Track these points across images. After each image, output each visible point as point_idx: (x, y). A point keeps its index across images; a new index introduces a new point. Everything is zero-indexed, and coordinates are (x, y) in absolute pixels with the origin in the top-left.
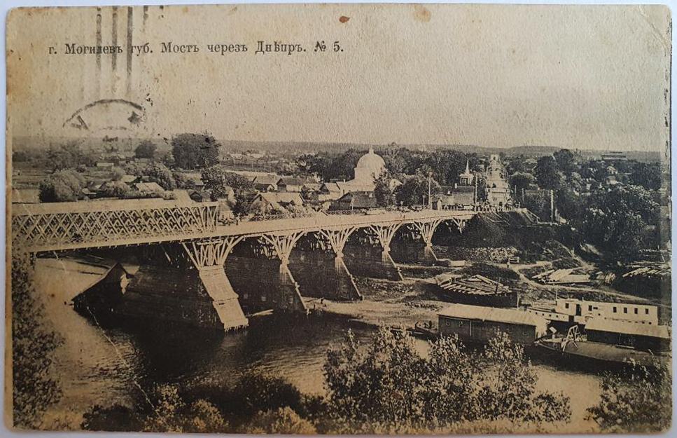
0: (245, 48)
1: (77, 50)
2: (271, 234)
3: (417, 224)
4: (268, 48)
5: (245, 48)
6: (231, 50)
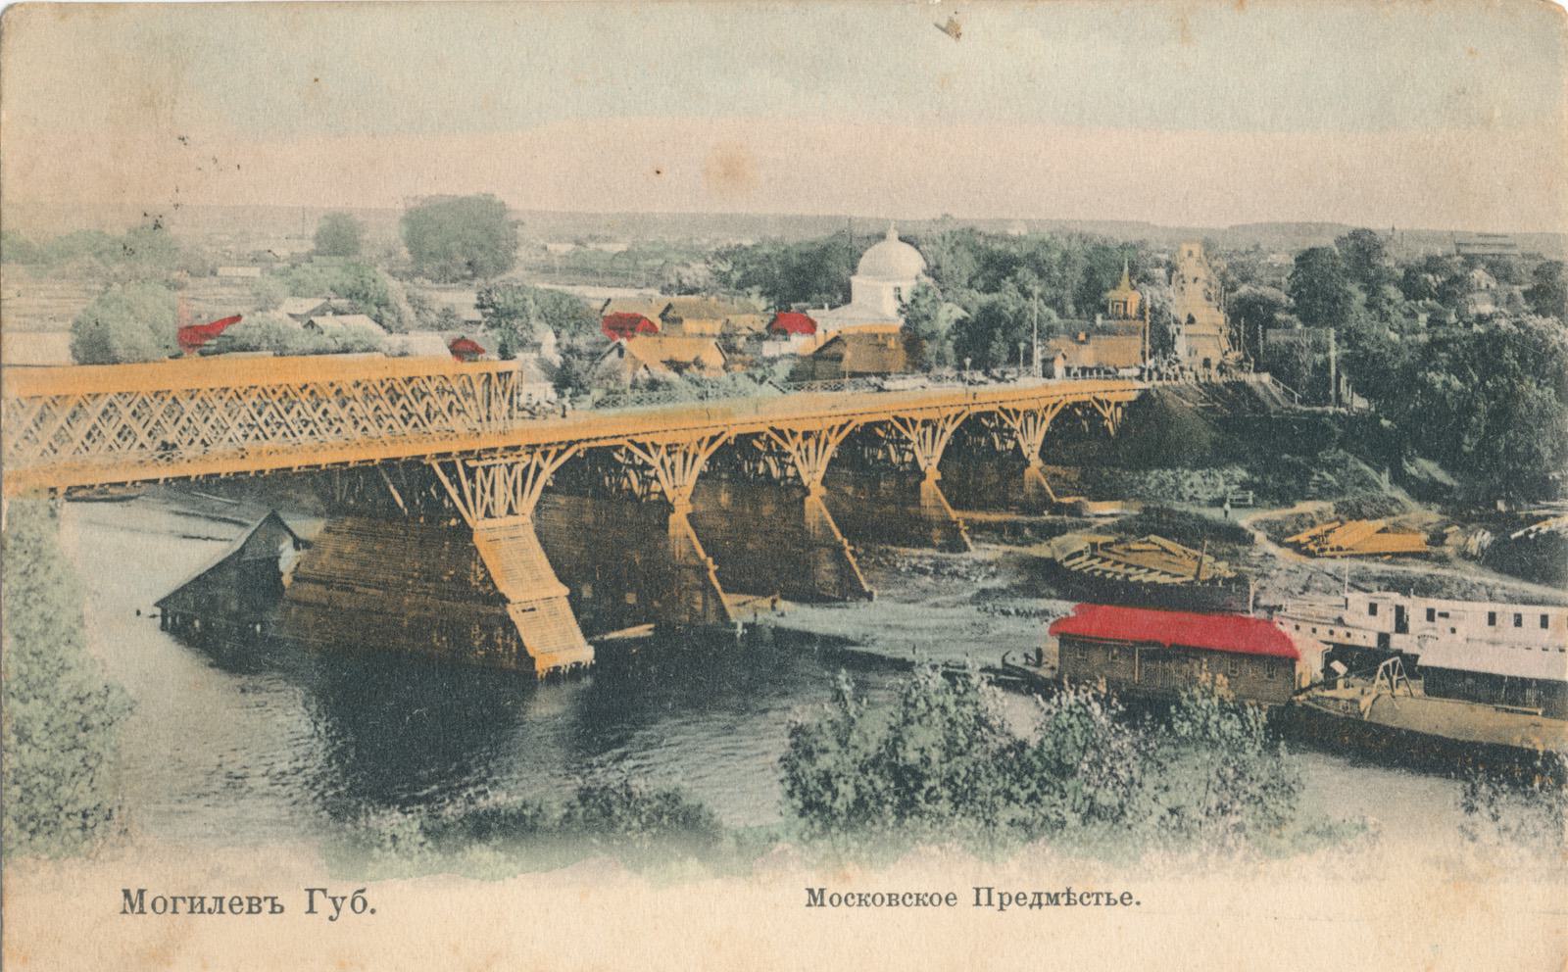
0: (277, 908)
1: (883, 899)
2: (647, 440)
3: (1007, 412)
5: (277, 908)
6: (237, 909)
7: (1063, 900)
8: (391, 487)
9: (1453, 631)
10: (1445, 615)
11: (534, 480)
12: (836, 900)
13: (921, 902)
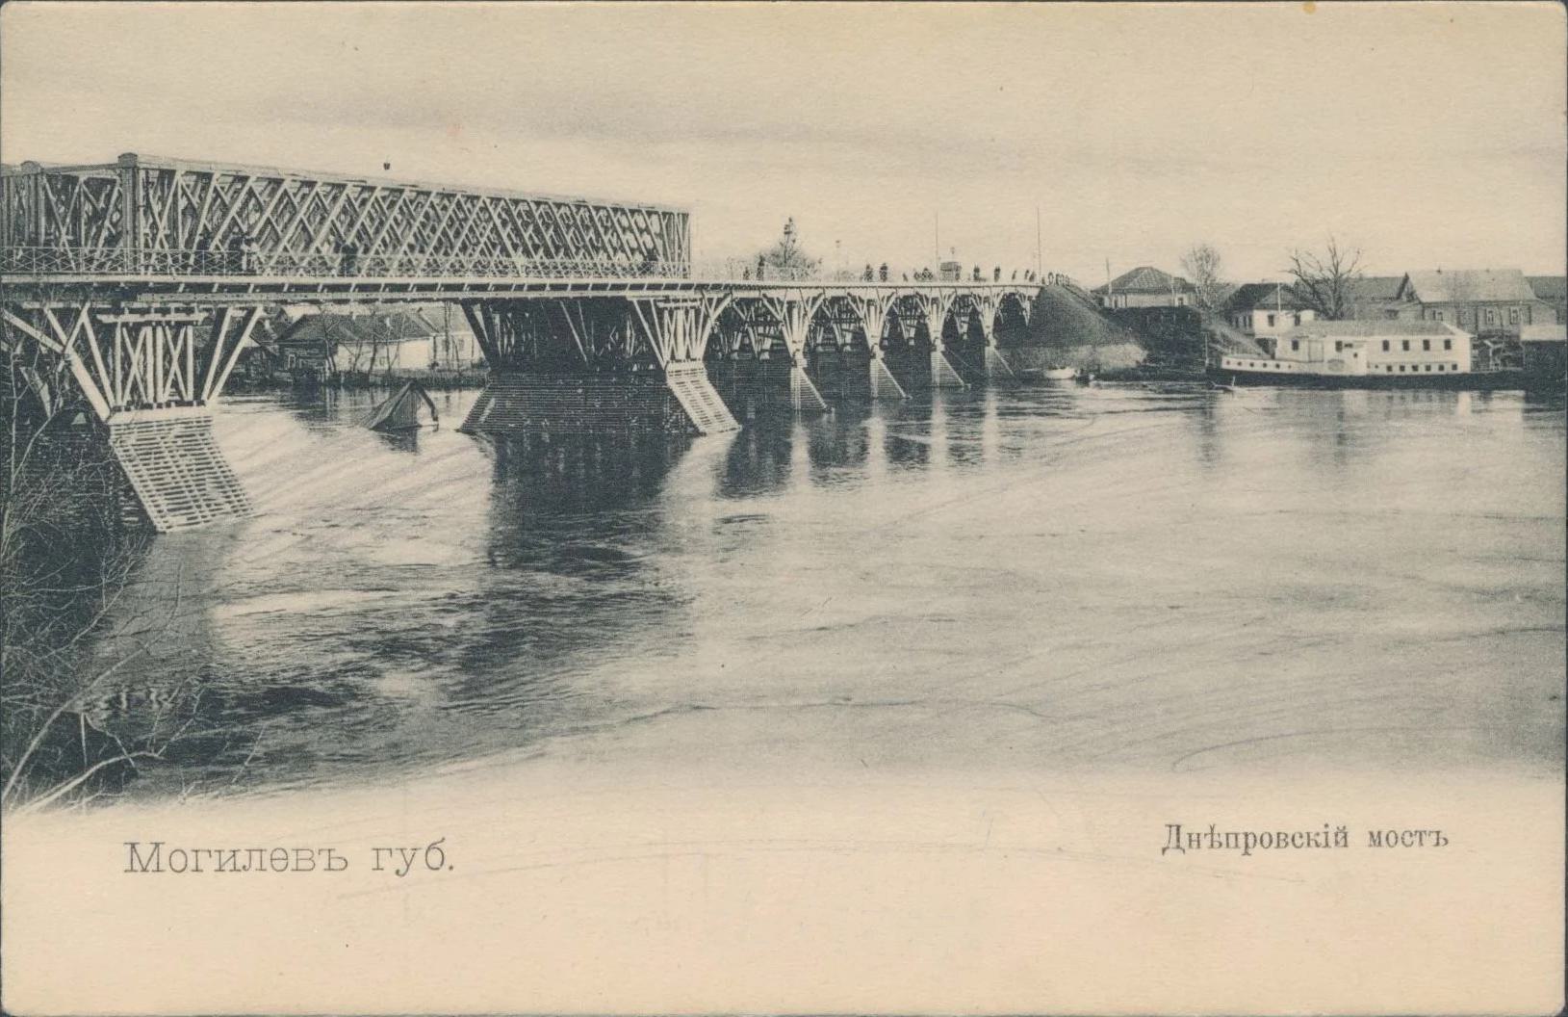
4: (1195, 840)
7: (1205, 842)
8: (574, 332)
9: (1356, 355)
10: (1350, 346)
11: (704, 327)
12: (1266, 839)
13: (1312, 843)
